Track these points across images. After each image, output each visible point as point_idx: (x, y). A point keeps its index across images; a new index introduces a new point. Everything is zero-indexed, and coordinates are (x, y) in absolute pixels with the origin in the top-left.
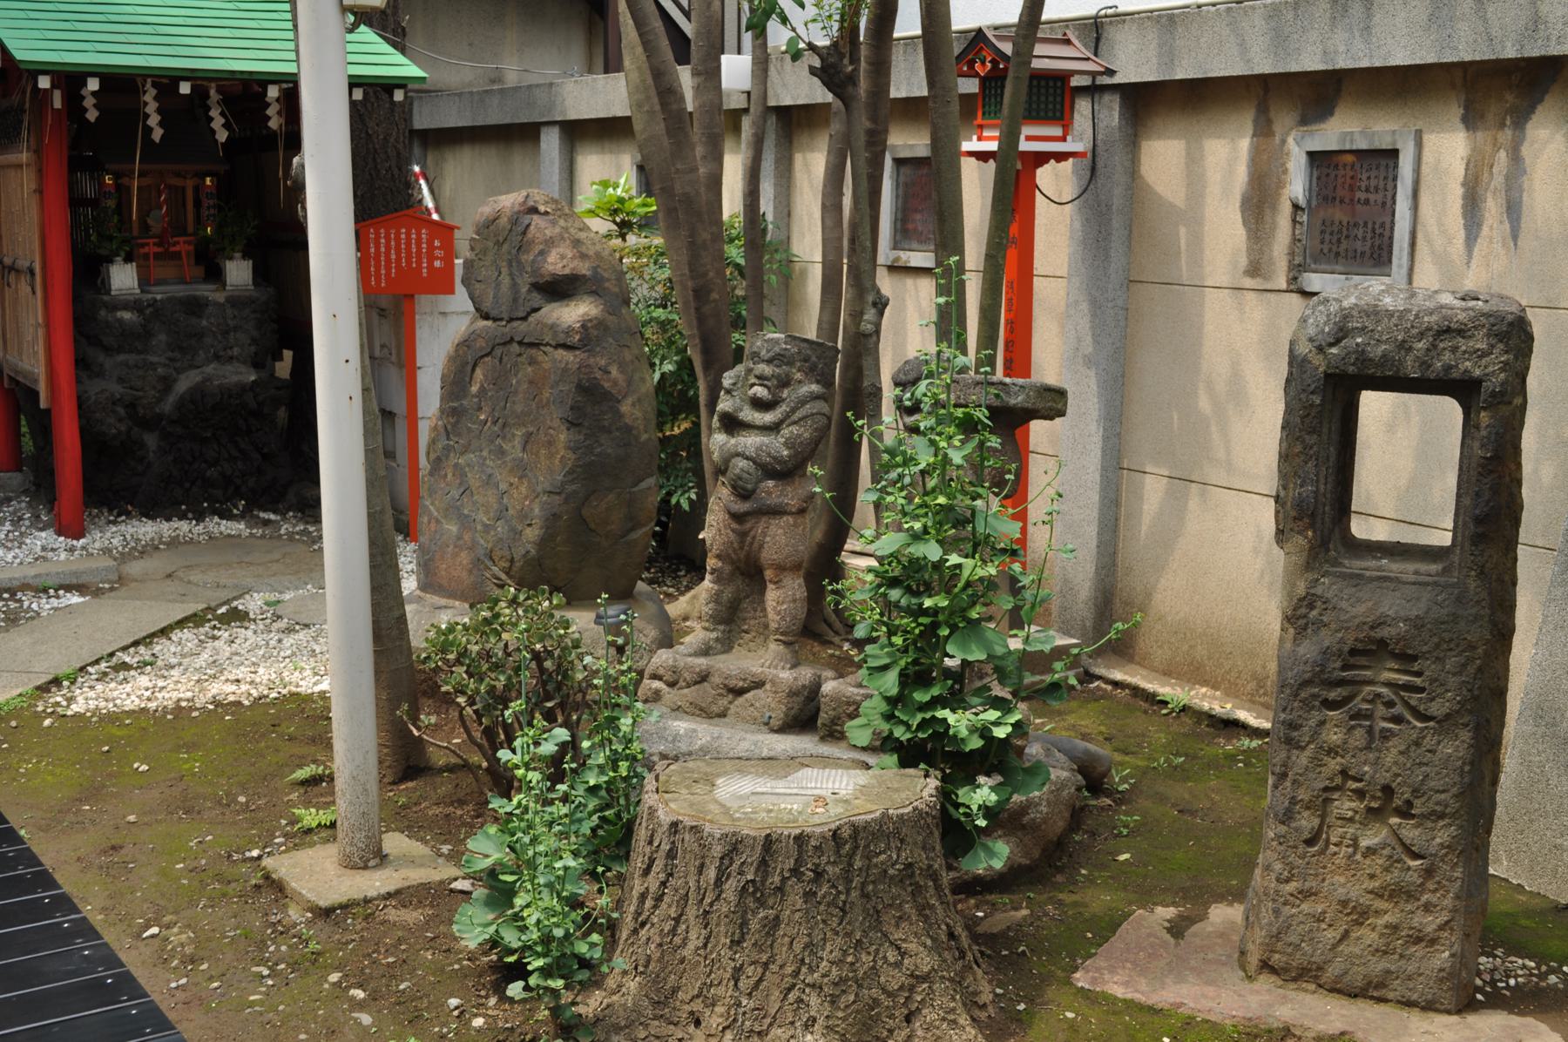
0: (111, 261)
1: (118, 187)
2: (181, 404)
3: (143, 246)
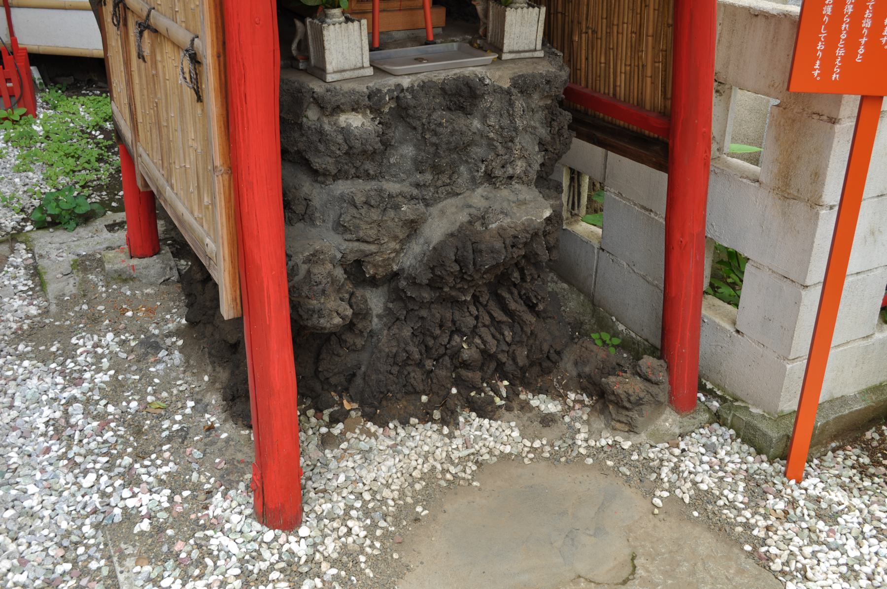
2: (435, 260)
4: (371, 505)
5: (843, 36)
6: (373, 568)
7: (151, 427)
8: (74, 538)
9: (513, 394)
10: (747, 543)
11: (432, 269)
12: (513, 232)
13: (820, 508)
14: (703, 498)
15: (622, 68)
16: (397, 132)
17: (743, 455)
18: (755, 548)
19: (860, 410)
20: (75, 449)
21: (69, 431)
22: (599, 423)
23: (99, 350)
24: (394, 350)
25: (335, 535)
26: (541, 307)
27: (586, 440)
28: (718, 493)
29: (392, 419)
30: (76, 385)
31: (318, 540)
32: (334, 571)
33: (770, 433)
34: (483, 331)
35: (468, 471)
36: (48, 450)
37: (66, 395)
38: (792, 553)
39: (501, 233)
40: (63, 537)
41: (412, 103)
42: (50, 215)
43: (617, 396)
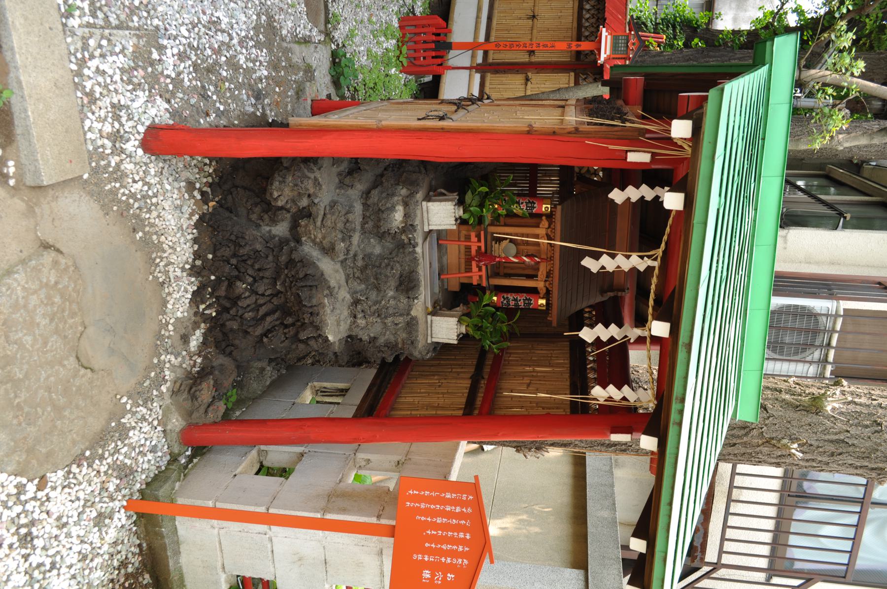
0: (461, 202)
1: (539, 216)
2: (306, 262)
3: (478, 236)
4: (148, 201)
5: (432, 507)
6: (110, 191)
7: (210, 79)
8: (152, 12)
9: (206, 318)
10: (91, 454)
11: (301, 261)
12: (321, 312)
13: (105, 518)
14: (123, 432)
15: (416, 400)
16: (389, 244)
17: (147, 472)
18: (87, 459)
19: (168, 566)
20: (203, 30)
21: (213, 29)
22: (180, 373)
23: (258, 64)
24: (247, 237)
25: (134, 171)
26: (265, 340)
27: (169, 362)
28: (126, 442)
29: (199, 233)
30: (239, 42)
31: (133, 159)
32: (113, 164)
33: (162, 490)
34: (253, 298)
35: (159, 275)
36: (204, 13)
37: (234, 35)
38: (80, 484)
39: (321, 305)
40: (154, 6)
41: (407, 251)
42: (340, 60)
43: (200, 384)
